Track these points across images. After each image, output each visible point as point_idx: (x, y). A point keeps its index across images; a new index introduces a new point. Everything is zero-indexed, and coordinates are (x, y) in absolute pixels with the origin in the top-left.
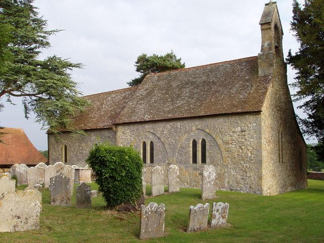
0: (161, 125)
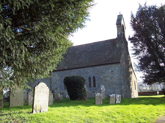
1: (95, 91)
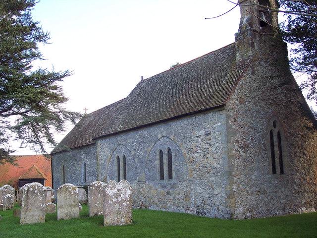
0: (131, 134)
1: (171, 190)
